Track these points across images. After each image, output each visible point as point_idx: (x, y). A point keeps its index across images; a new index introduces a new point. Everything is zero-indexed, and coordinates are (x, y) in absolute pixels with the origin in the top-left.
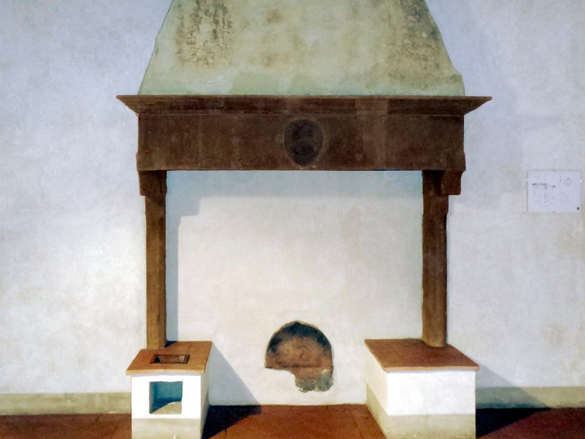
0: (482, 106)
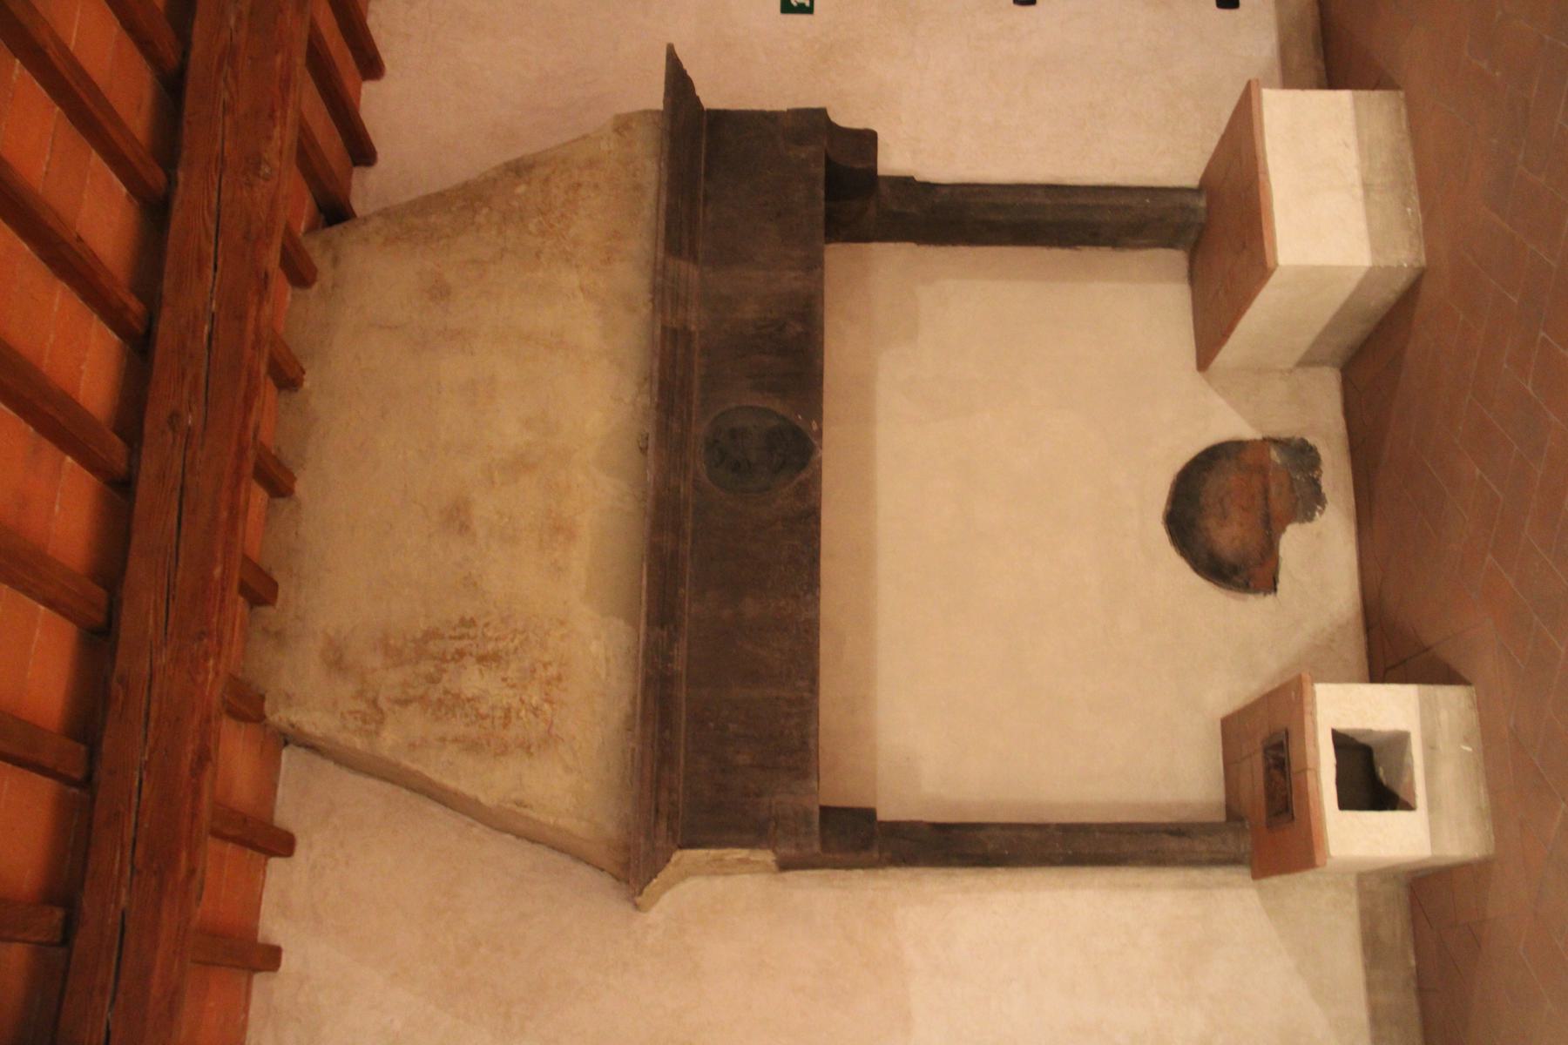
0: (685, 67)
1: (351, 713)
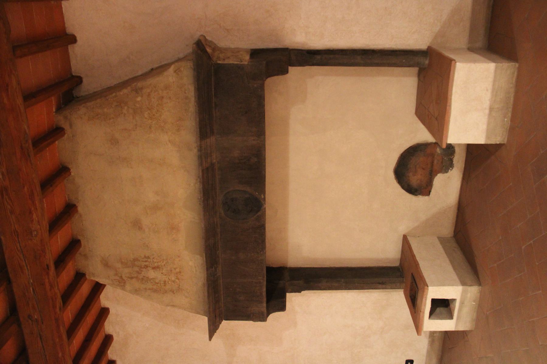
1: (115, 280)
